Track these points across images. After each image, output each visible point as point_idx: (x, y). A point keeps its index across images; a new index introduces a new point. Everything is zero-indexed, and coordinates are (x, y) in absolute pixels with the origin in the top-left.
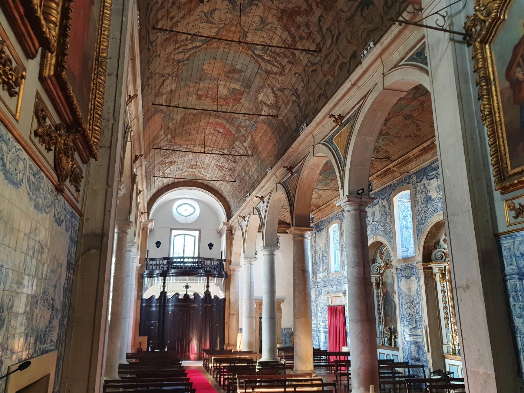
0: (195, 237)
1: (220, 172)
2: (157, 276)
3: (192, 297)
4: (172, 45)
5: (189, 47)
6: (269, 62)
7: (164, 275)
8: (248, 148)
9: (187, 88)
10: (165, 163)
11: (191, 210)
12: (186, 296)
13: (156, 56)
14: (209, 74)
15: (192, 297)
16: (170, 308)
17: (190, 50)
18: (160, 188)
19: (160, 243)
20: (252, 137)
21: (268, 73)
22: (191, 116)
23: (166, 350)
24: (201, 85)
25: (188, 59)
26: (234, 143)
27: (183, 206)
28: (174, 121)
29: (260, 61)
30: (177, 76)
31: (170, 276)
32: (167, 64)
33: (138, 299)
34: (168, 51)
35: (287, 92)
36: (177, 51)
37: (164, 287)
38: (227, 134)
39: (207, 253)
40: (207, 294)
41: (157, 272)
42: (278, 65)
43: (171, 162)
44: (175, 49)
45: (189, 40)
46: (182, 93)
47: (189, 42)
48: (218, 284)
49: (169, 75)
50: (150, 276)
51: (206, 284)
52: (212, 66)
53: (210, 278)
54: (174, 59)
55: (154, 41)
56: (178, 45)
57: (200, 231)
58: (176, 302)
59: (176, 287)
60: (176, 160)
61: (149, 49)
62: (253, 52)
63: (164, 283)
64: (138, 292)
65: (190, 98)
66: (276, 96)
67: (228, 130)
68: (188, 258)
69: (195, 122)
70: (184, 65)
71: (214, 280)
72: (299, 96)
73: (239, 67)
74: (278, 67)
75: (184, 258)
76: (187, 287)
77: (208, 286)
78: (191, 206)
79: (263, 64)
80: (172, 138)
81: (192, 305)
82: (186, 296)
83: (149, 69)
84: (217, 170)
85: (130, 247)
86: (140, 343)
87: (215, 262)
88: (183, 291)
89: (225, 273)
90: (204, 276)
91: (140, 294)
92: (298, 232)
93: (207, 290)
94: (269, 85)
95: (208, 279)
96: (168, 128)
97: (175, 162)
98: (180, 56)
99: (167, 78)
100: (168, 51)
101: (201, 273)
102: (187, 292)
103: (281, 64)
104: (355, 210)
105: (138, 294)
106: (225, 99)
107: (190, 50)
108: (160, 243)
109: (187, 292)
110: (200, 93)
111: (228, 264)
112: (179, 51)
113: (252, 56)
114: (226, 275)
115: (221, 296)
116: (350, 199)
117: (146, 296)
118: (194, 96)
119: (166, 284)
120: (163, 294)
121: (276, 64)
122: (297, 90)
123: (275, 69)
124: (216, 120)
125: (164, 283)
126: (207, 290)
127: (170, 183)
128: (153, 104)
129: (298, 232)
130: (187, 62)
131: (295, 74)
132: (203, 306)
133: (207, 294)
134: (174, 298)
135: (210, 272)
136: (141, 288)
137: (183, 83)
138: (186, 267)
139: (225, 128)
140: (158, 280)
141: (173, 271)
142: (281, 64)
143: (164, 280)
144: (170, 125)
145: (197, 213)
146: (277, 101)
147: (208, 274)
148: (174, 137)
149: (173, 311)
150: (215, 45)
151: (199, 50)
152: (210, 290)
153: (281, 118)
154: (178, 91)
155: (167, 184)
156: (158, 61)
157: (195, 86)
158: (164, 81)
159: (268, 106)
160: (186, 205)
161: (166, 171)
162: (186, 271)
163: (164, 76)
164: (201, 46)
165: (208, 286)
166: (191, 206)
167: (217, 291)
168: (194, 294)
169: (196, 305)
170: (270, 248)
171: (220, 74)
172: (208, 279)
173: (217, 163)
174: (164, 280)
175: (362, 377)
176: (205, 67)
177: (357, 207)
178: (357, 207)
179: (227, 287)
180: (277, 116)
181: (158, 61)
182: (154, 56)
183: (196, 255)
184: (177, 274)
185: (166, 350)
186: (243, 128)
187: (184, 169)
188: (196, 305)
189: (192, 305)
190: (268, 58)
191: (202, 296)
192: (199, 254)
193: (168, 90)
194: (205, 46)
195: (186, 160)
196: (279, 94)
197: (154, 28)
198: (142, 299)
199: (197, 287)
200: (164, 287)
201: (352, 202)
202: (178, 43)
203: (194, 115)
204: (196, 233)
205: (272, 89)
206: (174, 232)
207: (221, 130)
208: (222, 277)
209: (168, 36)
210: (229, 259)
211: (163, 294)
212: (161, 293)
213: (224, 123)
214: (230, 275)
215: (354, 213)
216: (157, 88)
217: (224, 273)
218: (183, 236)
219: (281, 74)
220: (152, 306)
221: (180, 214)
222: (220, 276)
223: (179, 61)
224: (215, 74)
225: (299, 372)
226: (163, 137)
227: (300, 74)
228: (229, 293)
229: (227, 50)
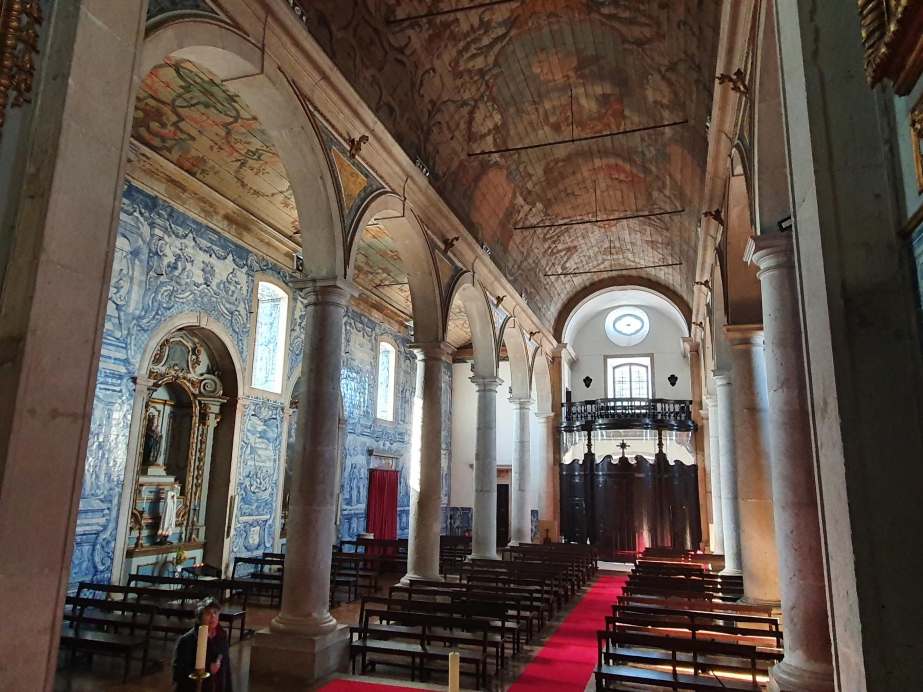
0: (647, 367)
1: (655, 253)
2: (578, 430)
3: (633, 462)
4: (450, 47)
5: (486, 41)
6: (632, 22)
7: (588, 428)
8: (673, 199)
9: (526, 118)
10: (559, 251)
11: (638, 324)
12: (623, 460)
13: (427, 72)
14: (550, 81)
15: (633, 462)
16: (601, 479)
17: (491, 45)
18: (571, 294)
19: (591, 380)
20: (670, 176)
21: (639, 43)
22: (560, 164)
23: (588, 543)
24: (548, 105)
25: (496, 63)
26: (650, 195)
27: (624, 319)
28: (534, 178)
29: (617, 25)
30: (493, 99)
31: (596, 429)
32: (459, 82)
33: (555, 465)
34: (446, 58)
35: (682, 68)
36: (466, 56)
37: (589, 446)
38: (633, 181)
39: (667, 392)
40: (661, 457)
41: (578, 423)
42: (647, 22)
43: (568, 249)
44: (460, 53)
45: (479, 28)
46: (521, 127)
47: (482, 32)
48: (679, 442)
49: (476, 101)
50: (570, 429)
51: (657, 442)
52: (546, 64)
53: (663, 432)
54: (469, 71)
55: (406, 45)
56: (462, 44)
57: (652, 356)
58: (609, 469)
59: (607, 446)
60: (575, 243)
61: (400, 62)
62: (600, 14)
63: (589, 439)
64: (554, 453)
65: (541, 132)
66: (670, 83)
67: (633, 175)
68: (640, 400)
69: (574, 173)
70: (496, 77)
71: (671, 436)
72: (699, 67)
73: (591, 52)
74: (650, 25)
75: (631, 399)
76: (623, 446)
77: (660, 445)
78: (636, 317)
79: (624, 29)
80: (546, 207)
81: (637, 475)
82: (623, 460)
83: (422, 96)
84: (651, 250)
85: (491, 385)
86: (547, 530)
87: (671, 406)
88: (617, 454)
89: (693, 422)
90: (652, 428)
91: (558, 456)
92: (738, 335)
93: (661, 450)
94: (651, 66)
95: (660, 434)
96: (529, 192)
97: (575, 247)
98: (479, 63)
99: (475, 107)
100: (446, 58)
101: (647, 424)
102: (623, 453)
103: (650, 17)
104: (777, 267)
105: (554, 457)
106: (600, 118)
107: (491, 45)
108: (591, 380)
109: (623, 453)
110: (552, 120)
111: (697, 408)
112: (469, 54)
113: (602, 23)
114: (696, 426)
115: (689, 460)
116: (762, 244)
117: (567, 459)
118: (546, 128)
119: (592, 442)
120: (589, 456)
121: (643, 20)
122: (692, 57)
123: (647, 32)
124: (605, 161)
125: (589, 439)
126: (661, 450)
127: (587, 283)
128: (469, 155)
129: (738, 335)
130: (496, 71)
131: (679, 26)
132: (654, 478)
133: (661, 457)
134: (605, 461)
135: (662, 421)
136: (557, 447)
137: (512, 110)
138: (626, 415)
139: (624, 171)
140: (580, 436)
141: (600, 421)
142: (650, 17)
143: (589, 435)
144: (529, 185)
145: (647, 328)
146: (675, 93)
147: (660, 425)
148: (548, 204)
149: (605, 482)
150: (530, 24)
151: (507, 44)
152: (664, 451)
153: (692, 122)
154: (511, 127)
155: (583, 285)
156: (437, 80)
157: (537, 110)
158: (471, 113)
159: (668, 107)
160: (628, 317)
161: (568, 265)
162: (623, 420)
163: (465, 104)
164: (505, 35)
165: (660, 445)
166: (636, 317)
167: (678, 450)
168: (636, 458)
169: (642, 475)
170: (726, 373)
171: (568, 77)
172: (660, 434)
173: (645, 238)
174: (589, 435)
175: (798, 627)
176: (537, 70)
177: (782, 259)
178: (782, 259)
179: (698, 445)
180: (687, 122)
181: (437, 80)
182: (420, 73)
183: (650, 397)
184: (609, 427)
185: (588, 543)
186: (651, 163)
187: (600, 258)
188: (642, 475)
189: (637, 475)
190: (627, 14)
191: (651, 459)
192: (654, 394)
193: (491, 127)
194: (513, 32)
195: (594, 242)
196: (668, 74)
197: (388, 23)
198: (561, 465)
199: (642, 446)
200: (589, 446)
201: (774, 249)
202: (459, 41)
203: (564, 161)
204: (646, 361)
205: (660, 72)
206: (611, 362)
207: (622, 177)
208: (689, 430)
209: (431, 32)
210: (697, 399)
211: (589, 456)
212: (585, 455)
213: (620, 162)
214: (703, 426)
215: (775, 272)
216: (463, 126)
217: (690, 423)
218: (628, 367)
219: (661, 36)
220: (599, 475)
221: (620, 332)
222: (682, 427)
223: (482, 73)
224: (559, 76)
225: (751, 602)
226: (527, 208)
227: (685, 23)
228: (703, 456)
229: (555, 27)
